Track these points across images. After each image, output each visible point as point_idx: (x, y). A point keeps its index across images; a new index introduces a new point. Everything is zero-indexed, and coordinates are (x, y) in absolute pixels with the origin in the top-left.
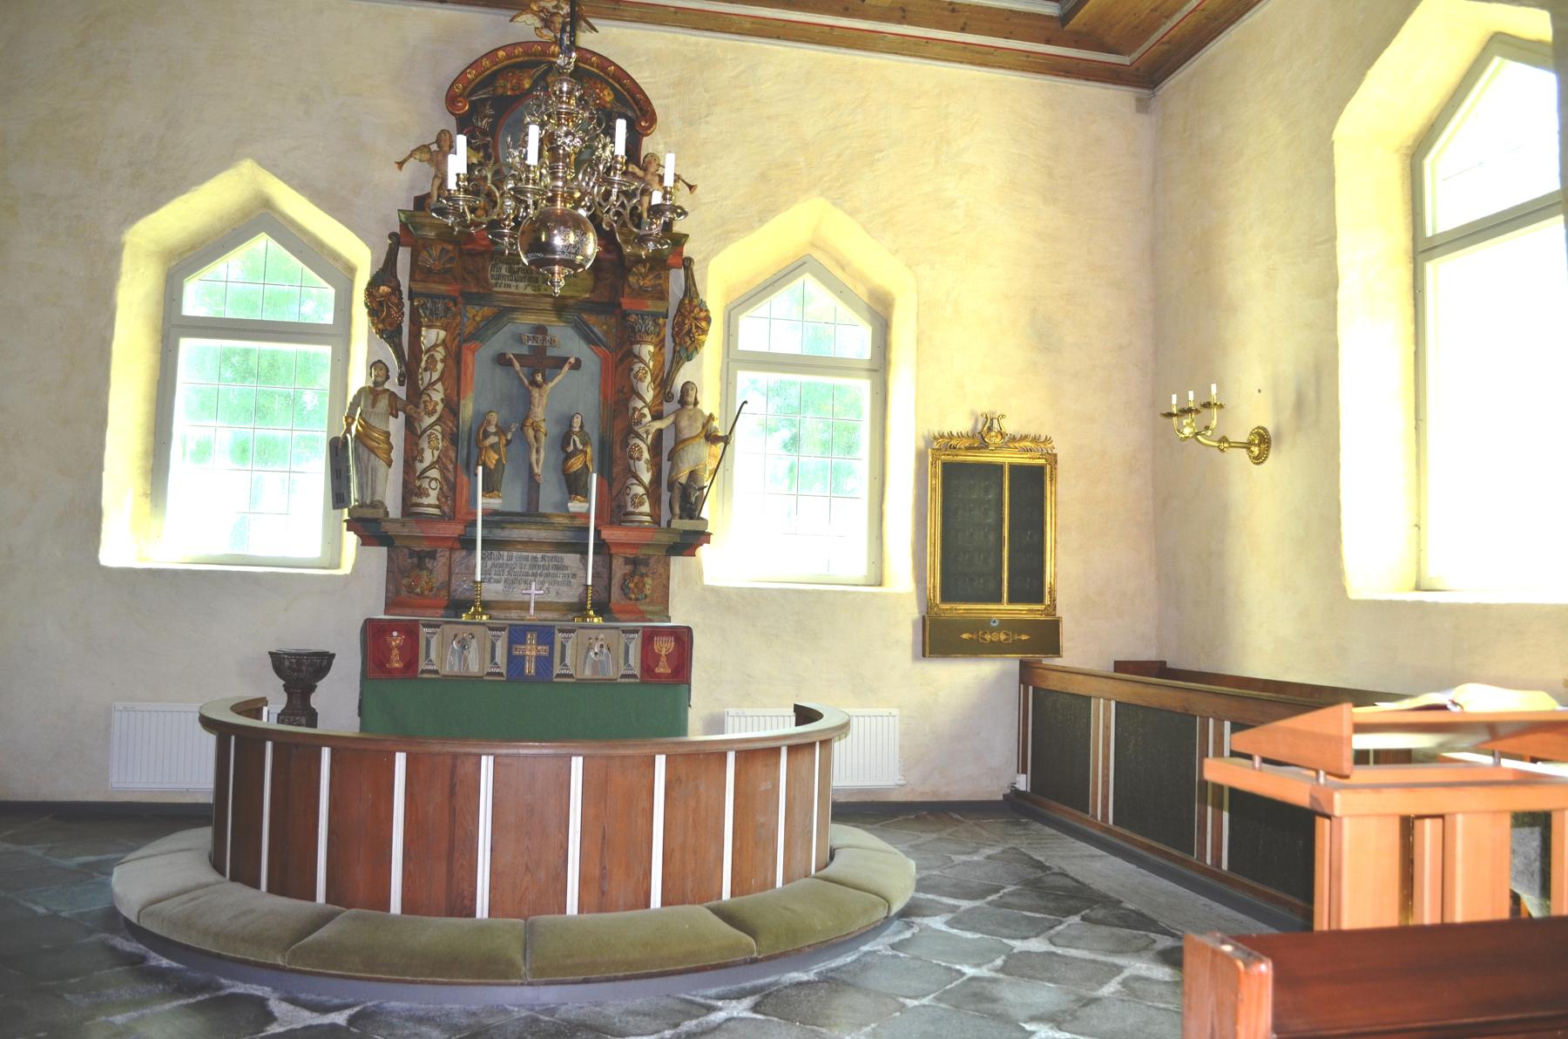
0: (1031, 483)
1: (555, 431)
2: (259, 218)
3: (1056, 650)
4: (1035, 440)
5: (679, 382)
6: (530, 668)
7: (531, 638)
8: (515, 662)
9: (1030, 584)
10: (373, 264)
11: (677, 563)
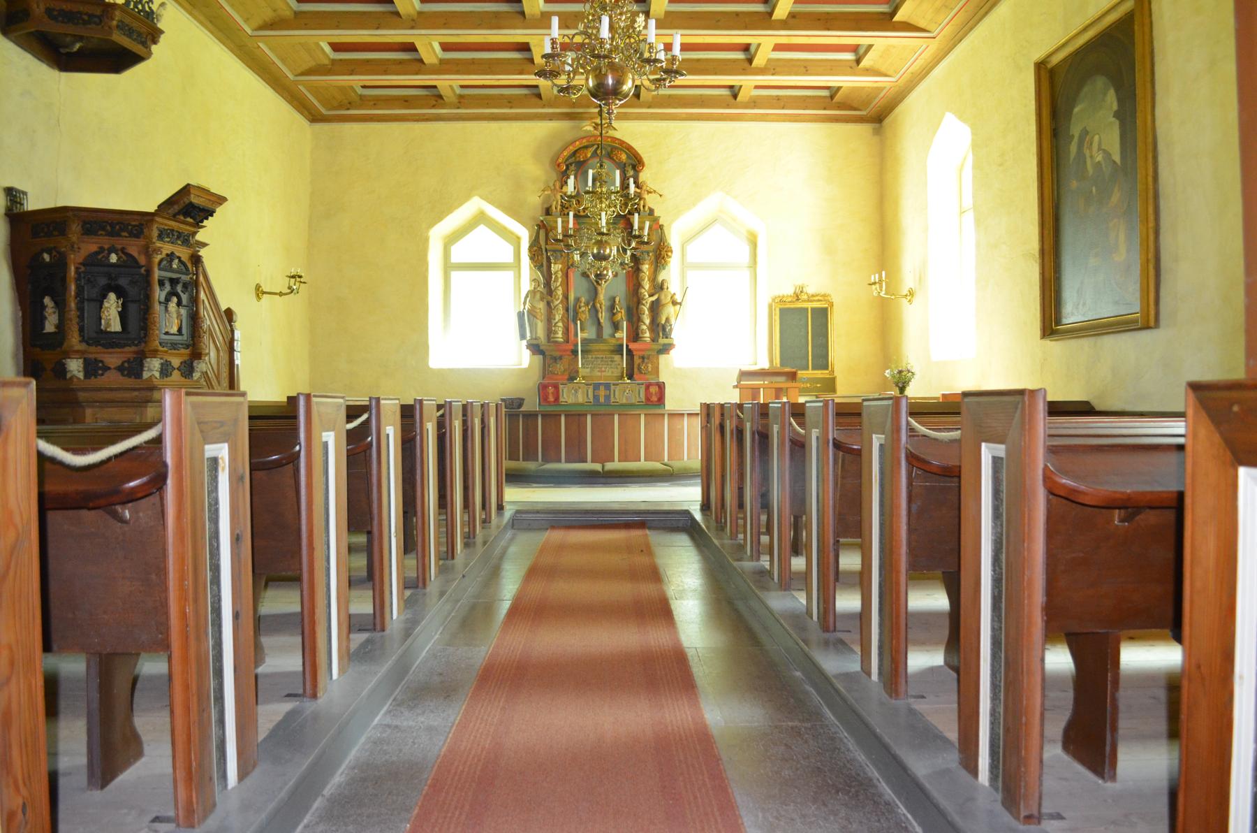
0: (822, 316)
1: (609, 304)
2: (481, 219)
3: (834, 390)
4: (824, 296)
5: (660, 278)
6: (602, 400)
7: (602, 388)
8: (596, 397)
9: (822, 360)
10: (530, 237)
11: (662, 358)
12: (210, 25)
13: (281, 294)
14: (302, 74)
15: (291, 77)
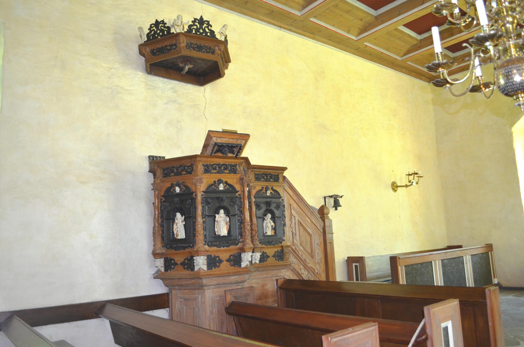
12: (330, 42)
13: (406, 186)
14: (405, 54)
15: (399, 58)
